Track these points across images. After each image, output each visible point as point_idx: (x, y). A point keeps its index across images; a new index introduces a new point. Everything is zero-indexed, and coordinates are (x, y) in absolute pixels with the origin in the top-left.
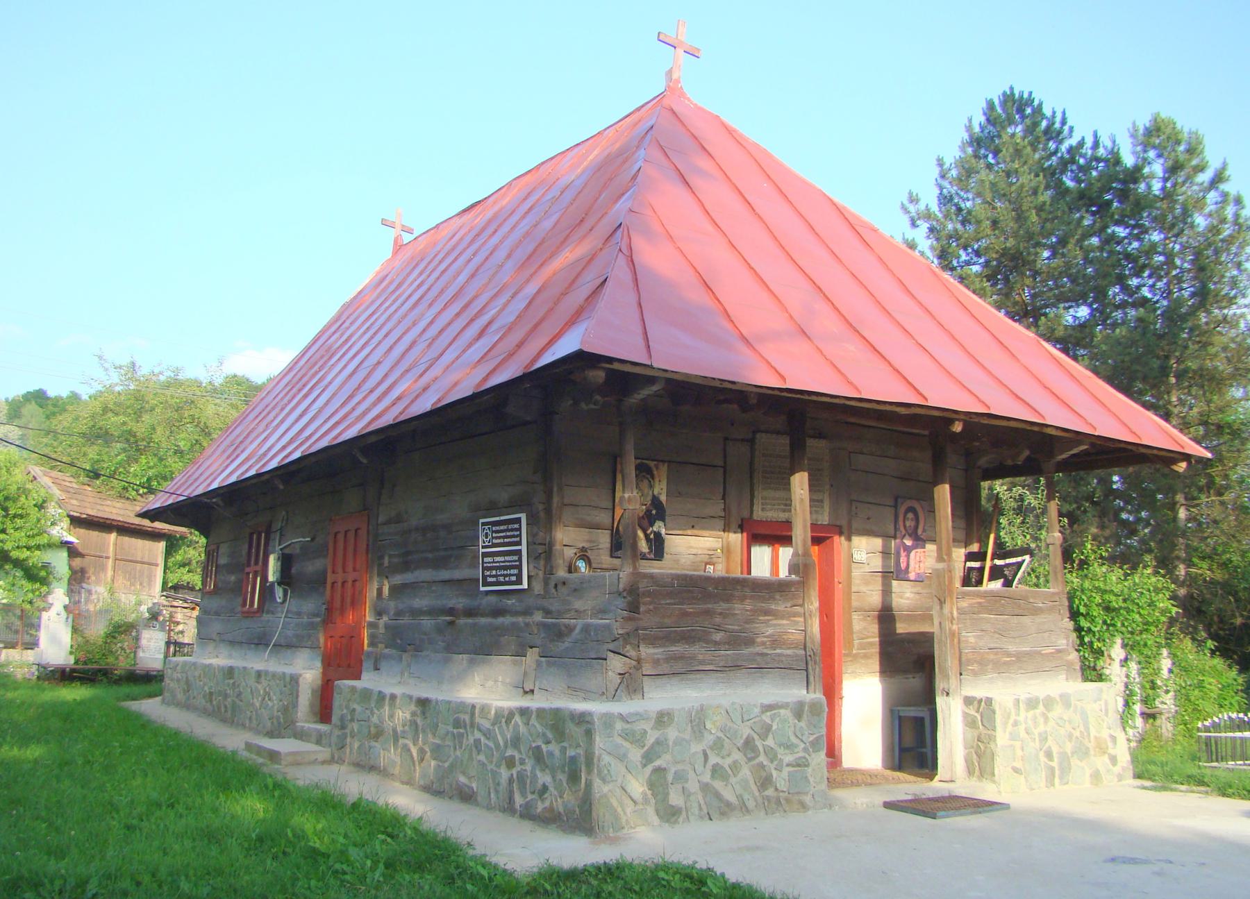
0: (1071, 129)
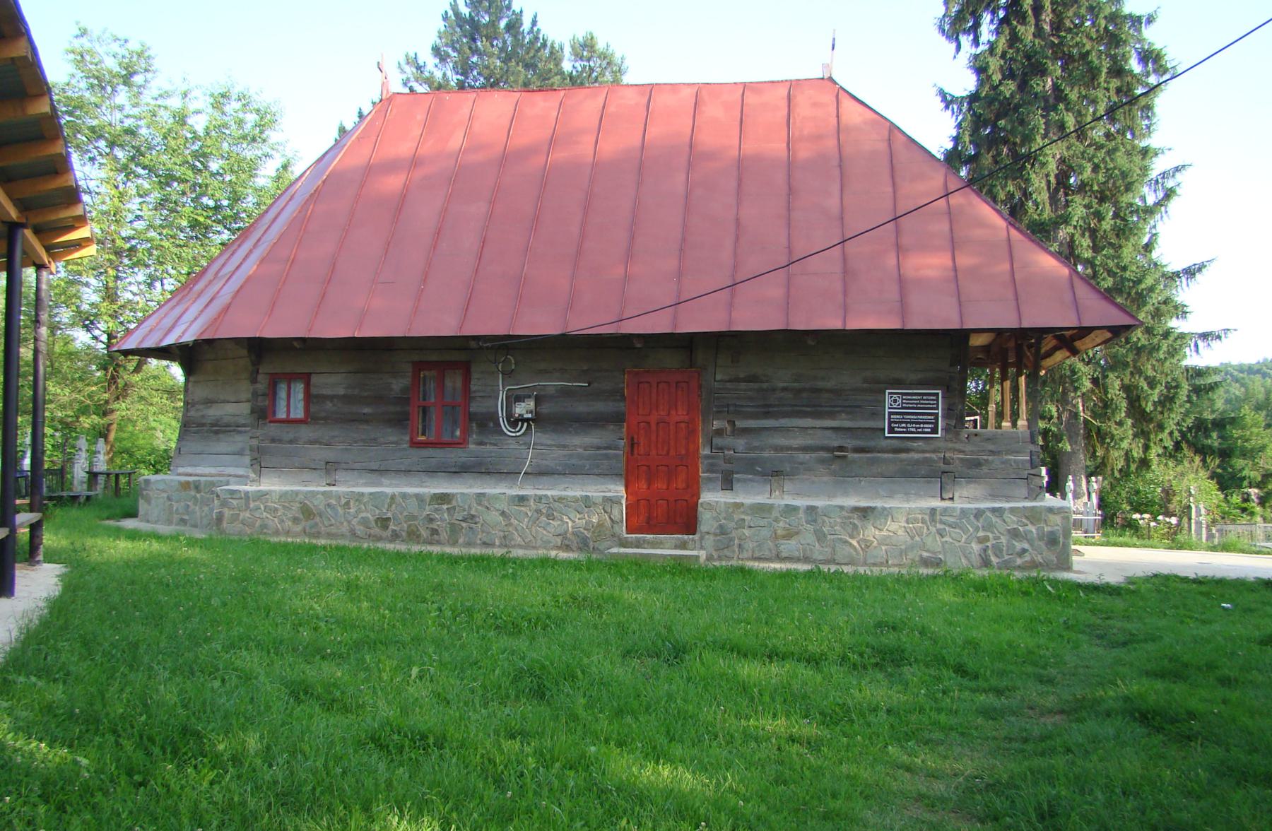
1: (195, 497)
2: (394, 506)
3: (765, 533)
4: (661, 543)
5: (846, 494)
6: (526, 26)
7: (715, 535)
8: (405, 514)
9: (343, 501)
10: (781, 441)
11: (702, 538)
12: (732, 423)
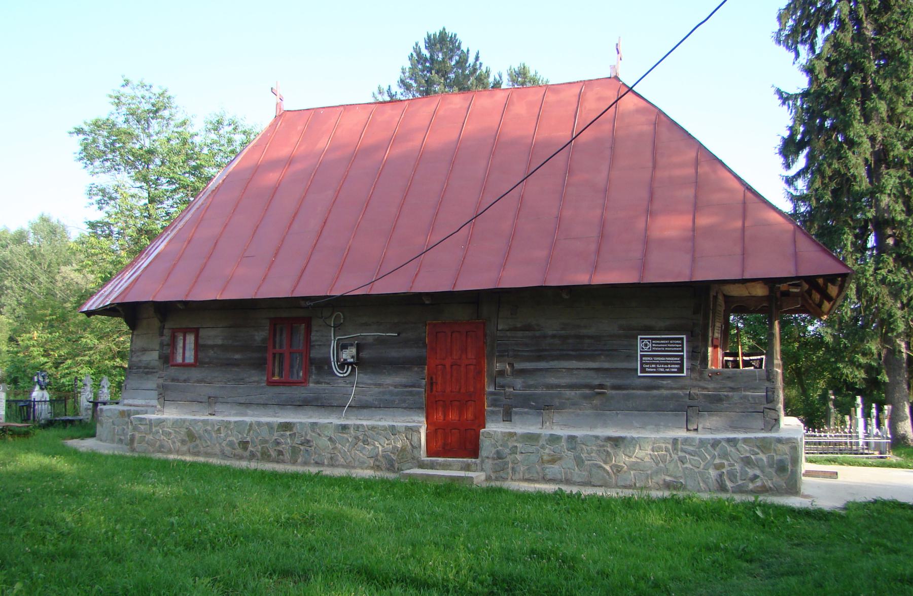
0: (481, 64)
3: (533, 458)
4: (450, 465)
5: (605, 425)
6: (471, 60)
7: (494, 459)
8: (260, 438)
9: (216, 428)
10: (552, 380)
11: (482, 462)
12: (512, 365)
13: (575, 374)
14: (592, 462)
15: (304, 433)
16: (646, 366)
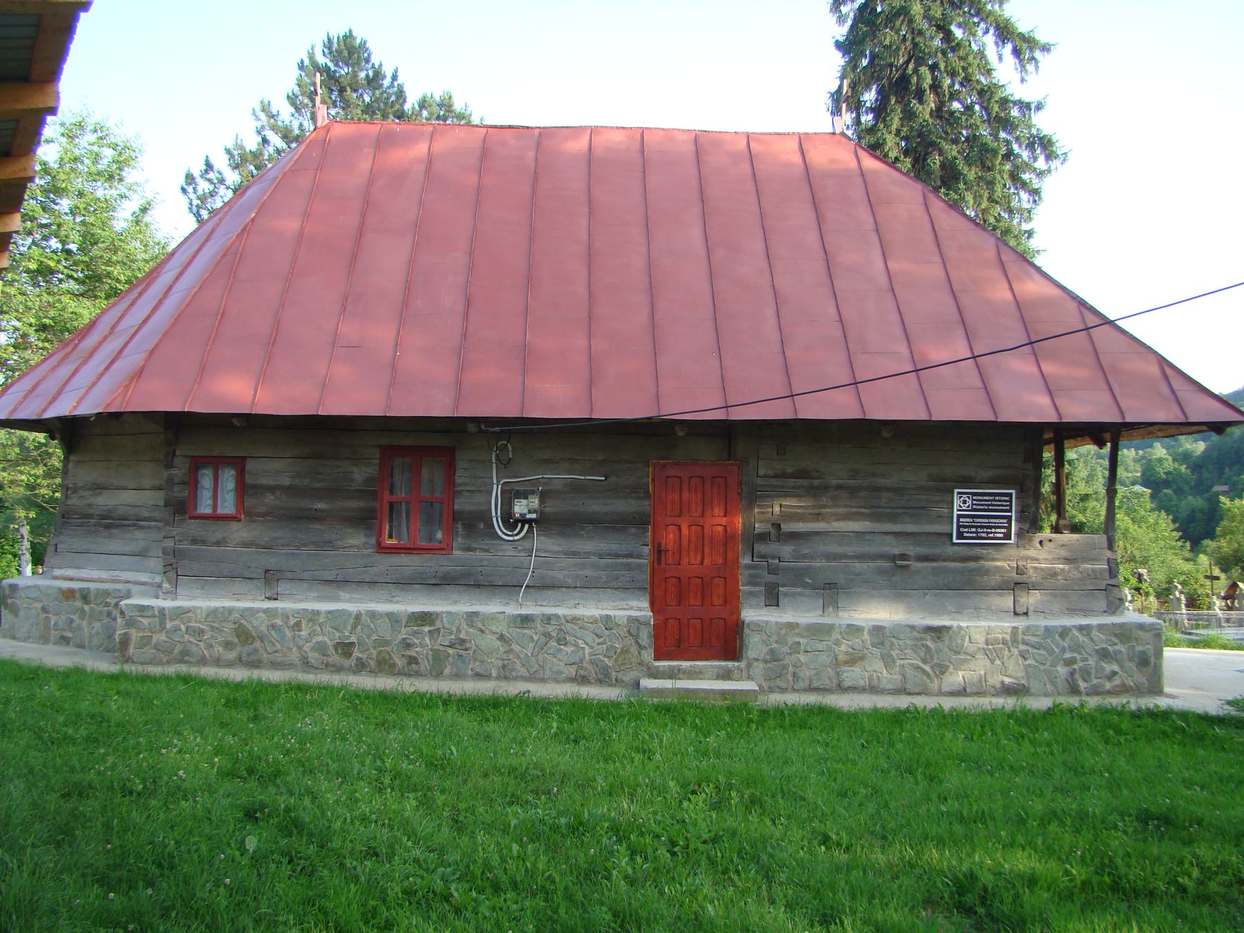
1: (83, 610)
2: (359, 628)
4: (701, 672)
7: (766, 662)
9: (292, 621)
11: (749, 666)
13: (868, 540)
14: (906, 661)
15: (454, 629)
16: (965, 530)
